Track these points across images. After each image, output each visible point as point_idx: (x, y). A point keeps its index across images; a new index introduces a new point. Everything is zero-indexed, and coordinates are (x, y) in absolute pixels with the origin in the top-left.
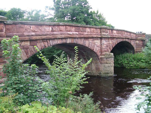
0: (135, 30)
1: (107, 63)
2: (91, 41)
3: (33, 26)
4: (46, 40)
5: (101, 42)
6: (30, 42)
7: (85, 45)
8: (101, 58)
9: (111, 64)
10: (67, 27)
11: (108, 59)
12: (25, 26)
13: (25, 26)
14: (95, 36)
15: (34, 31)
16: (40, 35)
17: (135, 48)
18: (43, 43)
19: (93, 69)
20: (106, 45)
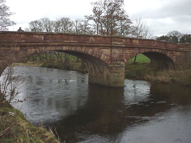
0: (54, 18)
1: (116, 73)
2: (96, 49)
3: (24, 35)
4: (37, 47)
5: (111, 51)
6: (20, 48)
7: (87, 53)
8: (110, 67)
9: (120, 74)
10: (69, 36)
11: (117, 68)
12: (34, 36)
13: (113, 50)
14: (102, 45)
15: (24, 39)
16: (30, 43)
17: (174, 61)
18: (66, 55)
19: (105, 77)
20: (118, 54)
